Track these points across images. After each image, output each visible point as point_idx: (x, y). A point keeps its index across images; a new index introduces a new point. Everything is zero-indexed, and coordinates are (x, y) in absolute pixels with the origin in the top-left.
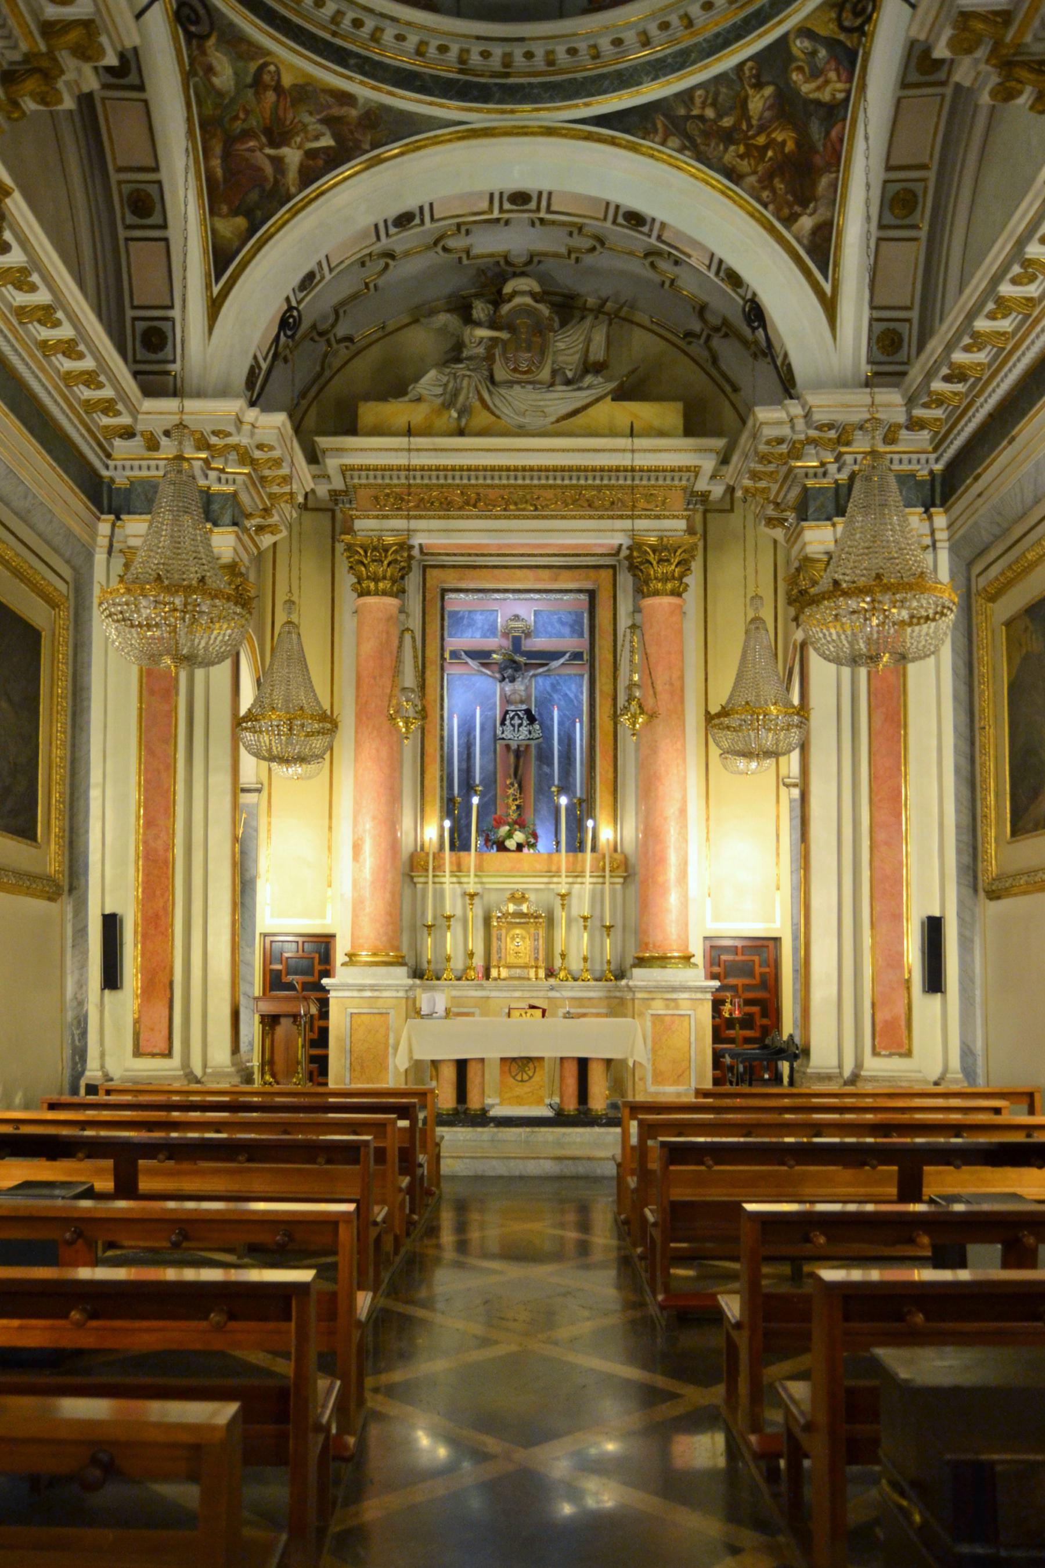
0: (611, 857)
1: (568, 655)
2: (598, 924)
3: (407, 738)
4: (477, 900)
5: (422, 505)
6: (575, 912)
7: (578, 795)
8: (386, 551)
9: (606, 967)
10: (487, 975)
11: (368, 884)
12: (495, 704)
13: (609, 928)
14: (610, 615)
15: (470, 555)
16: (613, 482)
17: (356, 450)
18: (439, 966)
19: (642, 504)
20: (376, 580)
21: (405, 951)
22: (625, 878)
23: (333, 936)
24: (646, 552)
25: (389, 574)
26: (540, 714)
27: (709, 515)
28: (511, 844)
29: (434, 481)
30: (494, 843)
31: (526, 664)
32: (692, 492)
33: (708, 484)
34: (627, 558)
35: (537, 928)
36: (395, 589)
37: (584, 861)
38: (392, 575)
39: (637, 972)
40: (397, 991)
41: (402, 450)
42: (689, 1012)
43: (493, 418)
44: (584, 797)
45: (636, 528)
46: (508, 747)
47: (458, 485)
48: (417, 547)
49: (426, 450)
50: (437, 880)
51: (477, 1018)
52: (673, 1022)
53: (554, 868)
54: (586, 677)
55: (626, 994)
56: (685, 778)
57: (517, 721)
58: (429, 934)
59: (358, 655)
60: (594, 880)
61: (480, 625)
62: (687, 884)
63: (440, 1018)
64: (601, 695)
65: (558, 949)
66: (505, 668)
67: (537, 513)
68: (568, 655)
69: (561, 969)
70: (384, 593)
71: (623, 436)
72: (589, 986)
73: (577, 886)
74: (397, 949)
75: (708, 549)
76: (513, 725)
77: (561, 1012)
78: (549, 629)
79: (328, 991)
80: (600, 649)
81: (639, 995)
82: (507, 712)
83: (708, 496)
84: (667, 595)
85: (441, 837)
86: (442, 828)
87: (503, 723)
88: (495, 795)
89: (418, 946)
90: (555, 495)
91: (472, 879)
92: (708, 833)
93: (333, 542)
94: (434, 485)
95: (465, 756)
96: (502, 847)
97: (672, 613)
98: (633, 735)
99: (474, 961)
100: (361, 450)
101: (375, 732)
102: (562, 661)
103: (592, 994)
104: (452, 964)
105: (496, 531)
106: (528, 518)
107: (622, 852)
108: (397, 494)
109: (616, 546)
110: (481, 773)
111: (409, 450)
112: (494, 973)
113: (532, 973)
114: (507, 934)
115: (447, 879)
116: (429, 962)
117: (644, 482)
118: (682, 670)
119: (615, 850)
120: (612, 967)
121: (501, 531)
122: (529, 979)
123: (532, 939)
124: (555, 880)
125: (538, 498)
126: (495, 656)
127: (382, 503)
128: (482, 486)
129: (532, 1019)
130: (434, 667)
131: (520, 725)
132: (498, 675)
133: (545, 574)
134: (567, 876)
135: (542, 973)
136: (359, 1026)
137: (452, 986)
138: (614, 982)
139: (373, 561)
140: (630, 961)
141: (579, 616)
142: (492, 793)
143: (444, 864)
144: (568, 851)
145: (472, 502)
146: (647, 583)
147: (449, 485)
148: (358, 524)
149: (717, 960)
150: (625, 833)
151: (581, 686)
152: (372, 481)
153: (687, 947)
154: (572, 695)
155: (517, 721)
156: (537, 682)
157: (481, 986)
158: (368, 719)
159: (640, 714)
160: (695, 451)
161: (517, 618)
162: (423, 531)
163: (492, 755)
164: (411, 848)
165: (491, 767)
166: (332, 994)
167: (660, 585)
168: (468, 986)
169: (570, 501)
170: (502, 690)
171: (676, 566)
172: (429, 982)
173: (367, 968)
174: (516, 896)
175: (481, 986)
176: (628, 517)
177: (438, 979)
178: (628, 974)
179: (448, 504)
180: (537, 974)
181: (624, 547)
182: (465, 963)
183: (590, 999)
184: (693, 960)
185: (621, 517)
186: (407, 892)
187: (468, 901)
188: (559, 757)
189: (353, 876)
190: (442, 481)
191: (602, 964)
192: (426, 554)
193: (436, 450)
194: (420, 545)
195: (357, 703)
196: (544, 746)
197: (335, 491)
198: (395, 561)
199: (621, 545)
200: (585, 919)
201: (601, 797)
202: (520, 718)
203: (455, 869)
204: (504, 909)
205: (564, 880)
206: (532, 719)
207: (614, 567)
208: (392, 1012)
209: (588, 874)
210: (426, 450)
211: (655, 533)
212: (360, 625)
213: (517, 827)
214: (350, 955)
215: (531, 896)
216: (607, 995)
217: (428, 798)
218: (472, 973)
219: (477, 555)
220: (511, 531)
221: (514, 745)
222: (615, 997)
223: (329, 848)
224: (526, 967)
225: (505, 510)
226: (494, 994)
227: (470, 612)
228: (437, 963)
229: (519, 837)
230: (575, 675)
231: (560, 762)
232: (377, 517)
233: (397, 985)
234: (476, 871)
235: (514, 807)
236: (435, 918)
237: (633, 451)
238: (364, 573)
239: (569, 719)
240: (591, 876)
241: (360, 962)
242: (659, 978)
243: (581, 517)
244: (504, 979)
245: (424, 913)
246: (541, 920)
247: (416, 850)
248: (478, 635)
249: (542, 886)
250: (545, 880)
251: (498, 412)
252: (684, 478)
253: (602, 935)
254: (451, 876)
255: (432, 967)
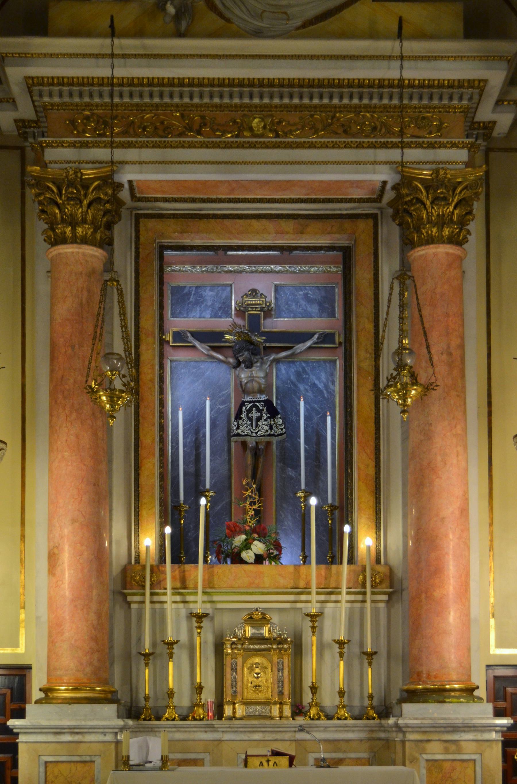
0: (372, 570)
1: (316, 336)
2: (356, 650)
3: (113, 417)
4: (205, 623)
5: (131, 131)
6: (328, 636)
7: (330, 501)
8: (86, 187)
9: (367, 702)
10: (219, 714)
11: (67, 602)
12: (229, 395)
13: (370, 656)
14: (370, 276)
15: (193, 200)
16: (375, 101)
17: (45, 55)
18: (161, 703)
19: (412, 129)
20: (73, 224)
21: (117, 685)
22: (390, 595)
23: (29, 668)
24: (417, 189)
25: (89, 217)
26: (283, 408)
27: (492, 155)
28: (248, 555)
29: (147, 100)
30: (227, 556)
31: (265, 348)
32: (473, 123)
33: (494, 111)
34: (390, 204)
35: (281, 656)
36: (98, 236)
37: (339, 574)
38: (94, 218)
39: (408, 708)
40: (105, 734)
41: (103, 56)
42: (473, 757)
43: (222, 22)
44: (337, 504)
45: (405, 160)
46: (244, 444)
47: (177, 106)
48: (126, 186)
49: (136, 56)
50: (156, 598)
51: (207, 769)
52: (454, 769)
53: (302, 584)
54: (339, 364)
55: (394, 734)
56: (466, 470)
57: (255, 414)
58: (147, 665)
59: (52, 319)
60: (352, 597)
61: (209, 303)
62: (469, 600)
63: (154, 769)
64: (358, 373)
65: (307, 681)
66: (240, 351)
67: (278, 140)
68: (316, 336)
69: (311, 706)
70: (84, 241)
71: (386, 37)
72: (346, 726)
73: (330, 605)
74: (105, 682)
75: (491, 199)
76: (251, 419)
77: (311, 757)
78: (294, 306)
79: (17, 734)
80: (357, 317)
81: (411, 737)
82: (243, 404)
83: (492, 129)
84: (443, 242)
85: (162, 547)
86: (162, 536)
87: (238, 417)
88: (230, 504)
89: (134, 681)
90: (301, 118)
91: (200, 597)
92: (491, 541)
93: (23, 188)
94: (147, 105)
95: (193, 458)
96: (237, 559)
97: (450, 266)
98: (403, 412)
99: (203, 696)
100: (51, 55)
101: (74, 415)
102: (309, 343)
103: (350, 736)
104: (175, 701)
105: (226, 163)
106: (267, 147)
107: (386, 563)
108: (99, 117)
109: (379, 185)
110: (211, 478)
111: (112, 56)
112: (228, 711)
113: (275, 710)
114: (243, 663)
115: (169, 598)
116: (147, 698)
117: (415, 102)
118: (462, 338)
119: (378, 561)
120: (375, 702)
121: (233, 163)
122: (272, 718)
123: (275, 669)
124: (303, 597)
125: (280, 122)
126: (227, 337)
127: (80, 129)
128: (207, 106)
129: (277, 769)
130: (150, 340)
131: (259, 419)
132: (231, 360)
133: (289, 225)
134: (318, 593)
135: (287, 710)
136: (56, 777)
137: (175, 727)
138: (377, 721)
139: (69, 199)
140: (395, 695)
141: (329, 291)
142: (227, 500)
143: (165, 579)
144: (319, 562)
145: (196, 127)
146: (418, 230)
147: (167, 105)
148: (50, 154)
149: (502, 693)
150: (389, 541)
151: (332, 375)
152: (66, 99)
153: (469, 676)
154: (321, 386)
155: (255, 414)
156: (278, 370)
157: (212, 726)
158: (65, 398)
159: (413, 384)
160: (481, 58)
161: (254, 293)
162: (133, 163)
163: (225, 456)
164: (124, 561)
165: (224, 470)
166: (22, 738)
167: (435, 230)
168: (195, 727)
169: (320, 127)
170: (237, 377)
171: (455, 208)
172: (146, 722)
173: (65, 707)
174: (255, 617)
175: (212, 726)
176: (394, 146)
177: (159, 718)
178: (396, 710)
179: (164, 130)
180: (281, 712)
181: (388, 187)
182: (191, 700)
183: (347, 741)
184: (476, 693)
185: (385, 146)
186: (119, 614)
187: (196, 624)
188: (306, 458)
189: (49, 593)
190: (157, 100)
191: (362, 698)
192: (140, 200)
193: (148, 56)
194: (130, 182)
195: (51, 380)
196: (288, 445)
197: (23, 121)
198: (98, 200)
199: (385, 183)
200: (341, 644)
201: (359, 498)
202: (259, 410)
203: (178, 585)
204: (240, 634)
205: (314, 597)
206: (273, 412)
207: (374, 217)
208: (98, 760)
209: (344, 590)
210: (136, 56)
211: (428, 166)
212: (54, 287)
213: (256, 536)
214: (46, 691)
215: (275, 619)
216: (369, 736)
217: (145, 499)
218: (201, 711)
219: (203, 201)
220: (245, 163)
221: (251, 442)
222: (379, 739)
223: (22, 562)
224: (267, 703)
225: (237, 136)
226: (227, 737)
227: (198, 287)
228: (156, 699)
229: (258, 547)
230: (325, 361)
231: (306, 464)
232: (72, 145)
233: (104, 727)
234: (204, 587)
235: (252, 513)
236: (154, 644)
237: (402, 58)
238: (59, 216)
239: (318, 413)
240: (348, 593)
241: (57, 698)
242: (436, 715)
243: (335, 146)
244: (241, 719)
245: (140, 640)
246: (286, 646)
247: (130, 562)
248: (208, 314)
249: (287, 605)
250: (292, 598)
251: (228, 15)
252: (466, 97)
253: (362, 664)
254: (173, 594)
255: (151, 704)
